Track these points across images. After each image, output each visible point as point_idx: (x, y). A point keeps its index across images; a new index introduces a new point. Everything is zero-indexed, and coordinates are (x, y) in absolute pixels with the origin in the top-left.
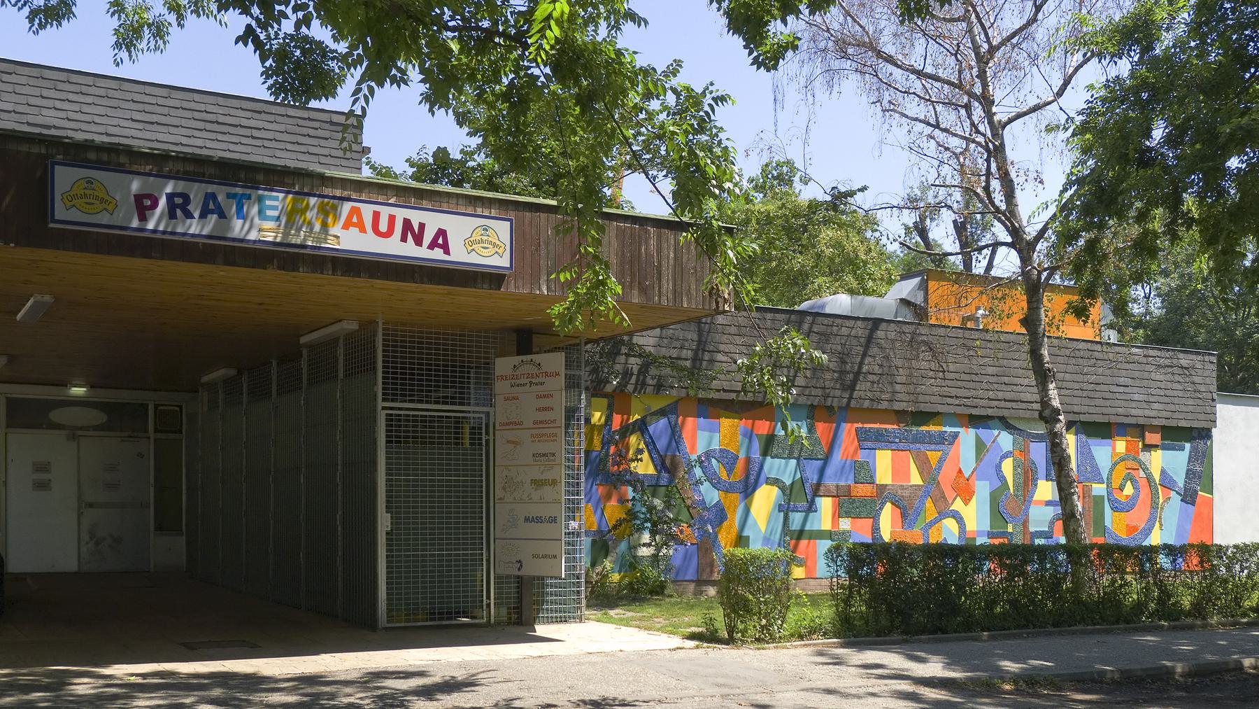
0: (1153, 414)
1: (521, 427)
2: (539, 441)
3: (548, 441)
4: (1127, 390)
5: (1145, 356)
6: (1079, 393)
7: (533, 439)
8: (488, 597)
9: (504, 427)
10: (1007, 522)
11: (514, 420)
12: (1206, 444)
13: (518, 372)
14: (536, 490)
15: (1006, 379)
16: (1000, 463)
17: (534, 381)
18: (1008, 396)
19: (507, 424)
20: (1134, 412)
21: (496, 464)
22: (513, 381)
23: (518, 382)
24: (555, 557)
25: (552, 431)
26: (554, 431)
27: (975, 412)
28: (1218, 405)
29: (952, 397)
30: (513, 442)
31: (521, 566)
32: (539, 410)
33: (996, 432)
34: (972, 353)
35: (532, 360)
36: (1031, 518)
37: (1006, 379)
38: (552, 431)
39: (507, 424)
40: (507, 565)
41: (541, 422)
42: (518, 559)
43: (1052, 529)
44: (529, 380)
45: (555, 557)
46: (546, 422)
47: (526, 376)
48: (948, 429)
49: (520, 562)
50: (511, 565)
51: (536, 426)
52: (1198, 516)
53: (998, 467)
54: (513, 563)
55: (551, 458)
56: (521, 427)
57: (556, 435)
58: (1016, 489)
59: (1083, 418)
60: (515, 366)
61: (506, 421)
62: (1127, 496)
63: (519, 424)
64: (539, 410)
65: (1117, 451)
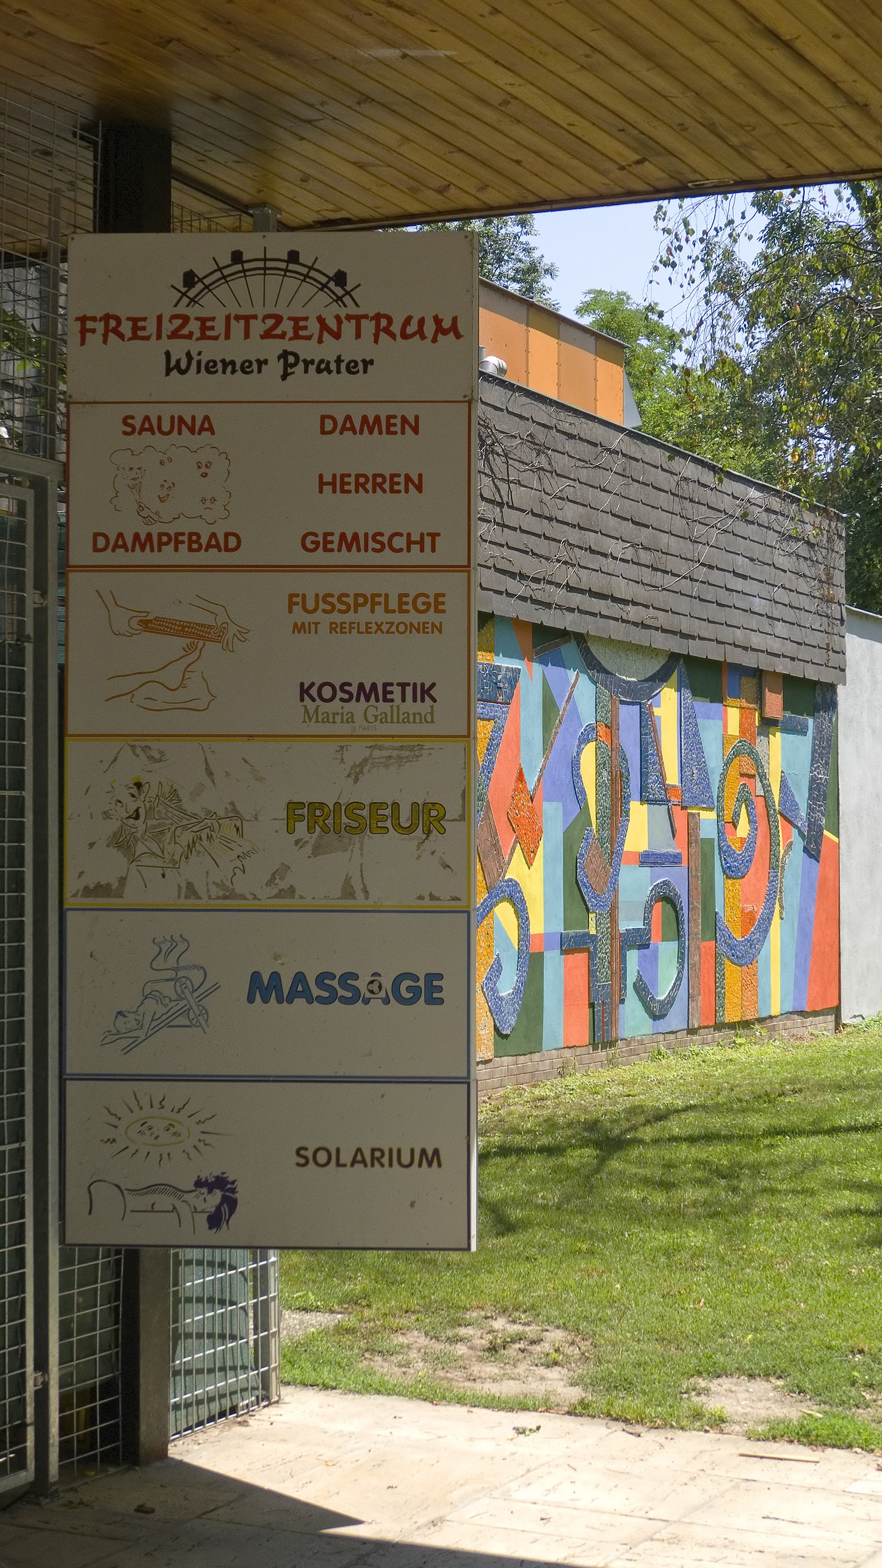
0: (775, 645)
1: (427, 558)
2: (333, 627)
3: (391, 629)
4: (738, 584)
5: (768, 510)
6: (685, 585)
7: (299, 616)
8: (42, 1364)
9: (121, 557)
10: (588, 910)
11: (185, 526)
12: (831, 719)
13: (209, 306)
14: (317, 851)
15: (591, 539)
16: (578, 754)
17: (306, 350)
18: (587, 580)
19: (142, 542)
20: (756, 640)
21: (71, 729)
22: (178, 349)
23: (211, 351)
24: (432, 1158)
25: (413, 584)
26: (431, 584)
27: (550, 619)
28: (848, 636)
29: (512, 575)
30: (181, 629)
31: (230, 1203)
32: (339, 484)
33: (572, 674)
34: (543, 461)
35: (293, 257)
36: (621, 898)
37: (591, 539)
38: (413, 584)
39: (142, 542)
40: (135, 1202)
41: (350, 542)
42: (210, 1172)
43: (649, 924)
44: (278, 346)
45: (432, 1158)
46: (381, 542)
47: (258, 327)
48: (504, 662)
49: (220, 1182)
50: (164, 1201)
51: (320, 558)
52: (824, 880)
53: (575, 765)
54: (177, 1192)
55: (409, 706)
56: (427, 558)
57: (438, 603)
58: (601, 826)
59: (696, 649)
60: (190, 279)
61: (131, 526)
62: (742, 840)
63: (213, 543)
64: (339, 484)
65: (729, 733)
